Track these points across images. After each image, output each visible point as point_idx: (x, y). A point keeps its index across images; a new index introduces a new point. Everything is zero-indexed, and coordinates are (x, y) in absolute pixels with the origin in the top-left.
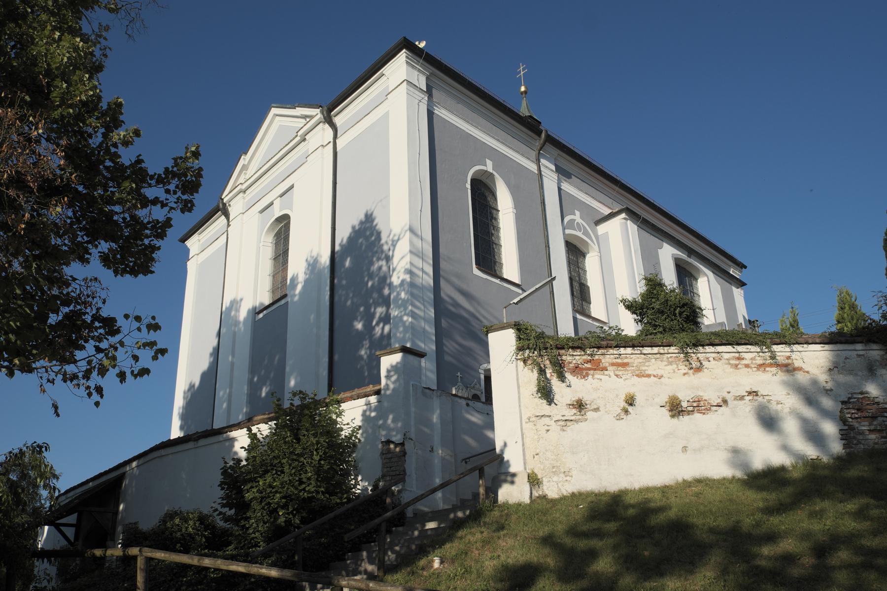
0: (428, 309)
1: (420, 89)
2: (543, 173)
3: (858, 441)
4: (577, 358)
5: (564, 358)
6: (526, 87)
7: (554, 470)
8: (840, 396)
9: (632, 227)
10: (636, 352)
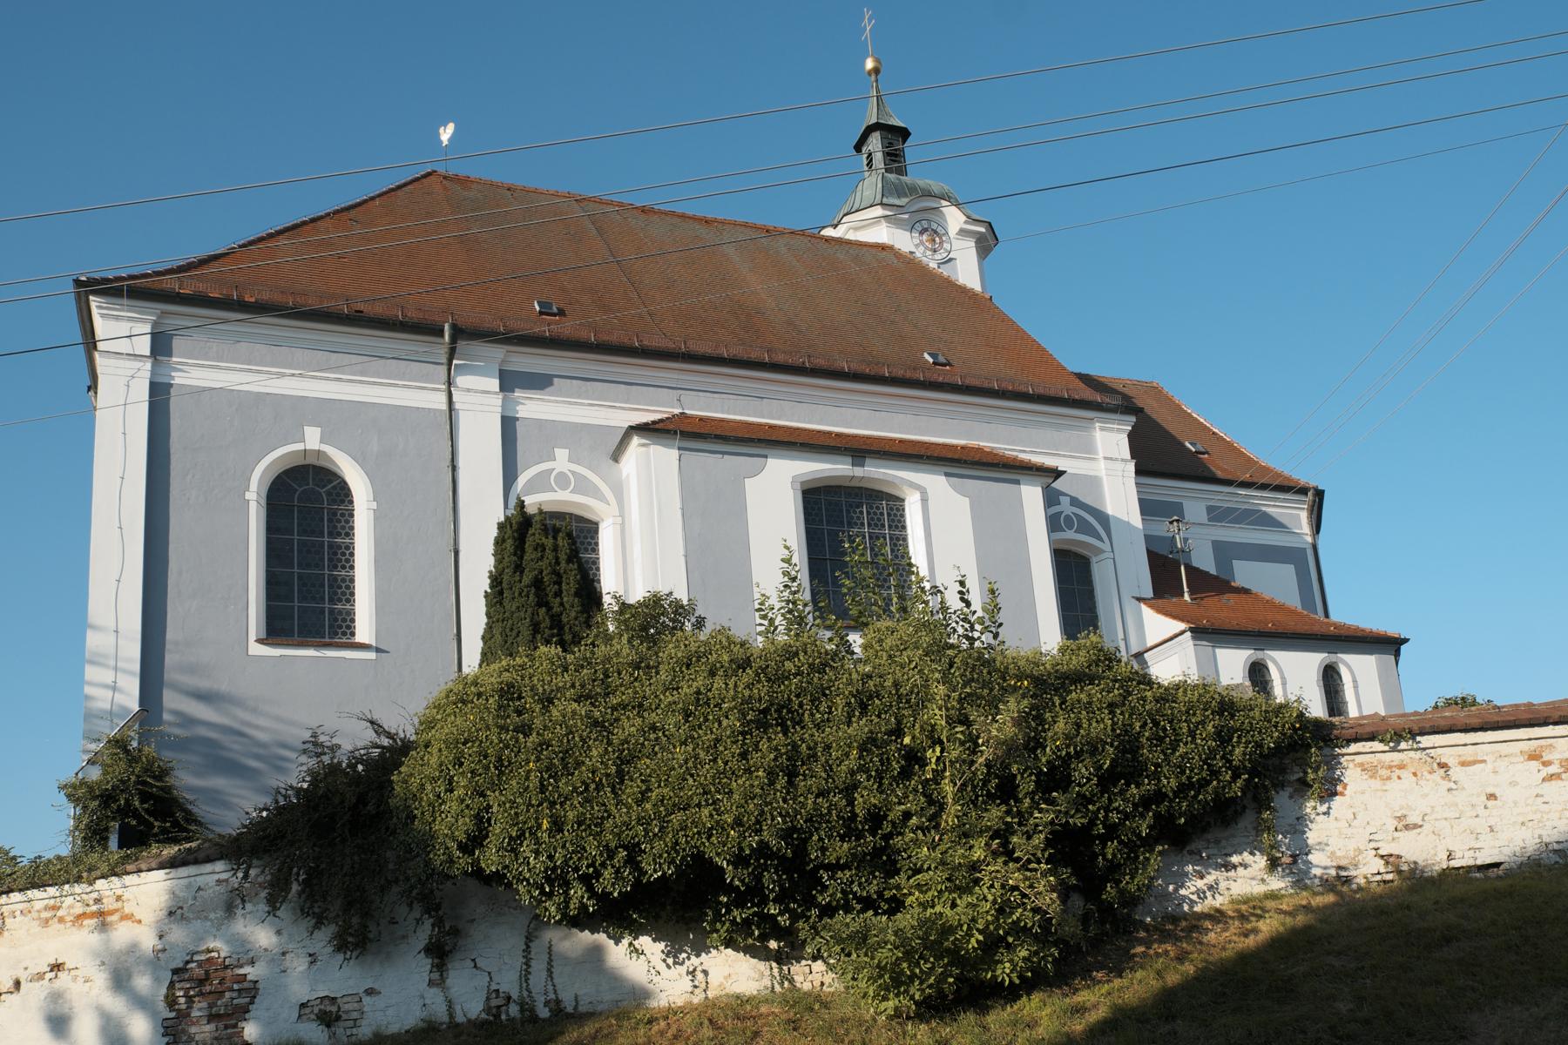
2: (457, 406)
6: (877, 60)
9: (665, 457)
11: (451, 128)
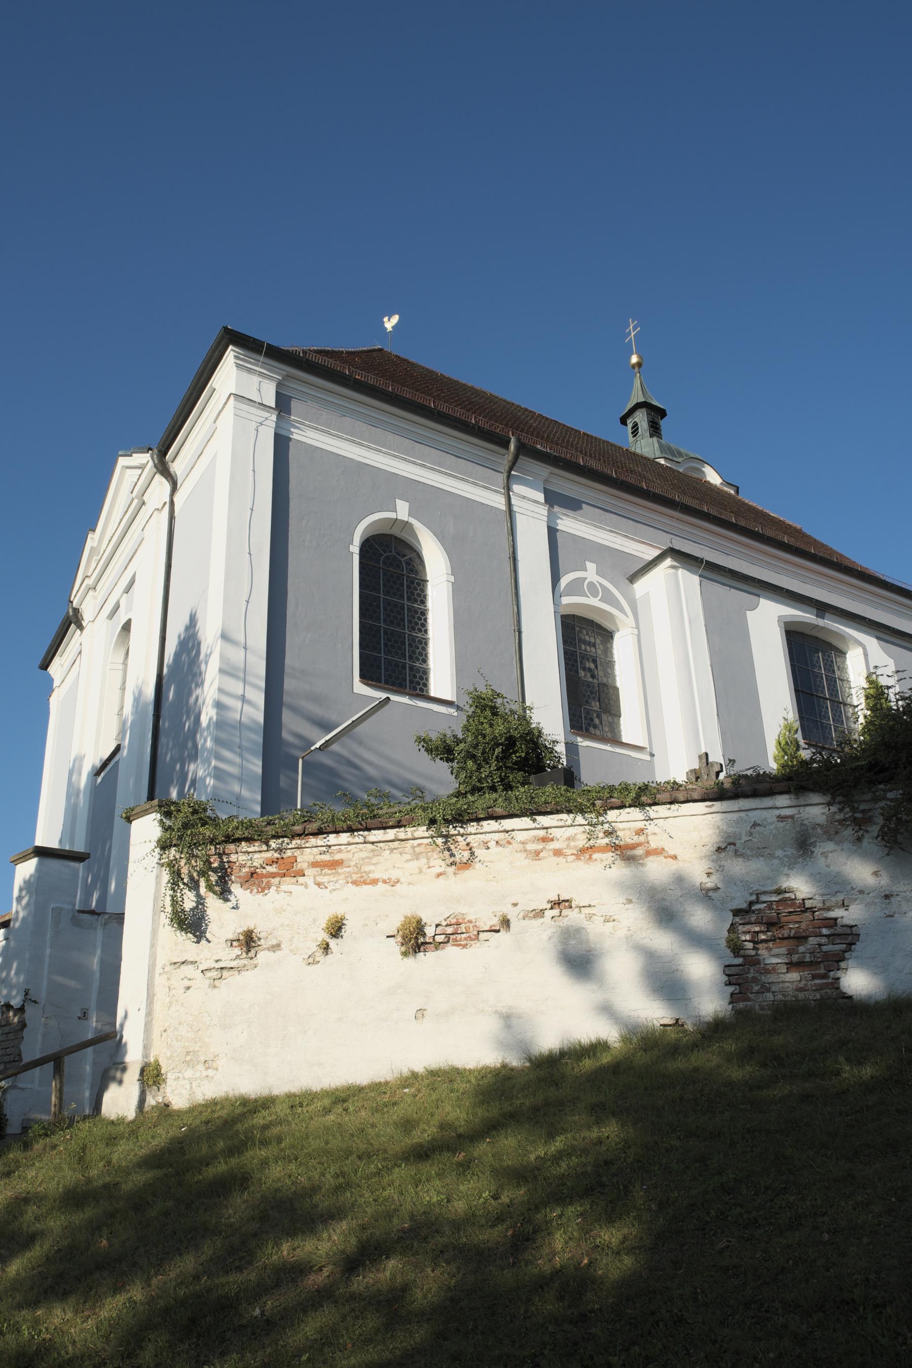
0: (248, 761)
1: (262, 404)
2: (515, 509)
3: (763, 986)
4: (257, 856)
5: (233, 858)
6: (640, 357)
7: (188, 1058)
8: (733, 899)
9: (689, 580)
10: (357, 840)
11: (395, 319)
